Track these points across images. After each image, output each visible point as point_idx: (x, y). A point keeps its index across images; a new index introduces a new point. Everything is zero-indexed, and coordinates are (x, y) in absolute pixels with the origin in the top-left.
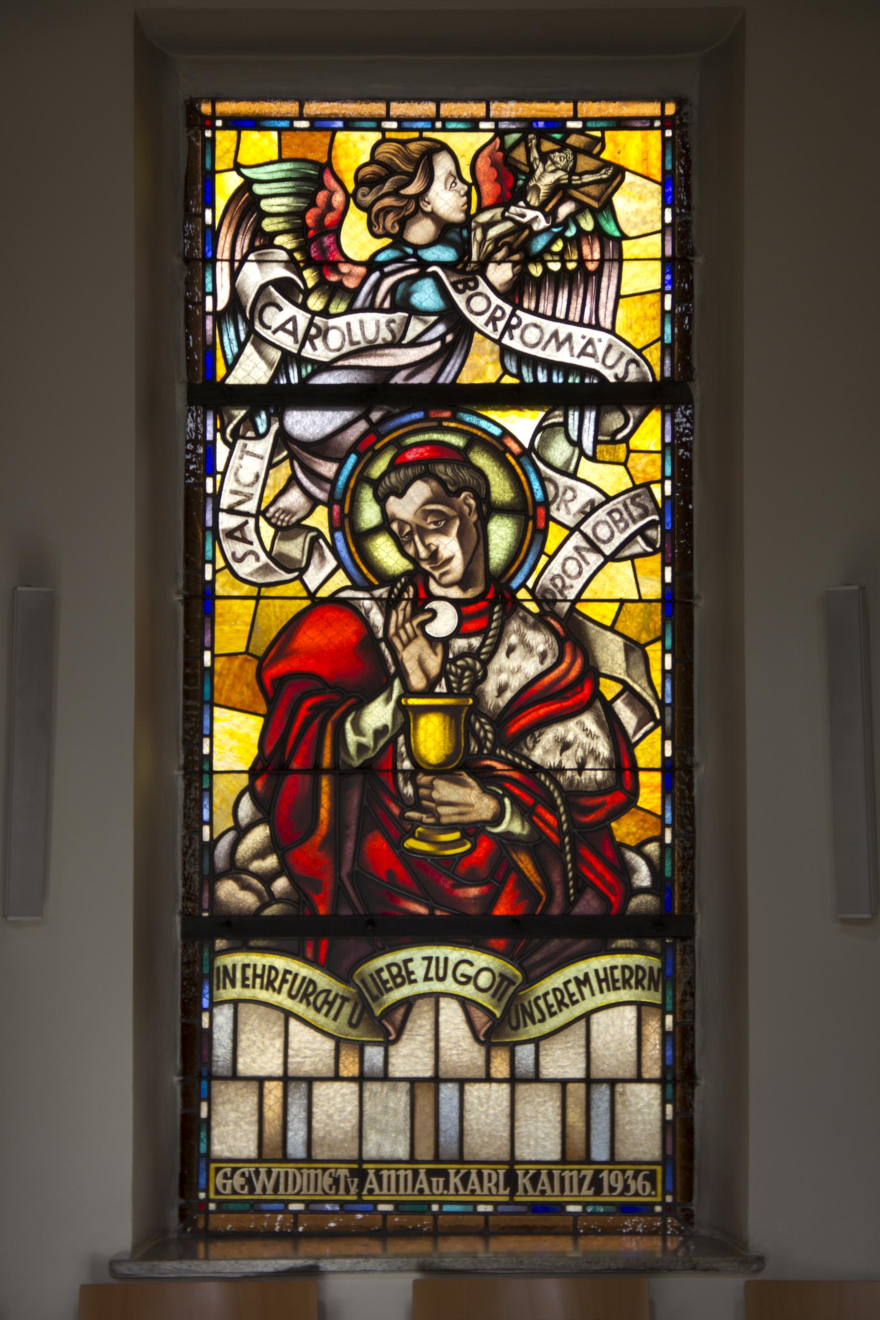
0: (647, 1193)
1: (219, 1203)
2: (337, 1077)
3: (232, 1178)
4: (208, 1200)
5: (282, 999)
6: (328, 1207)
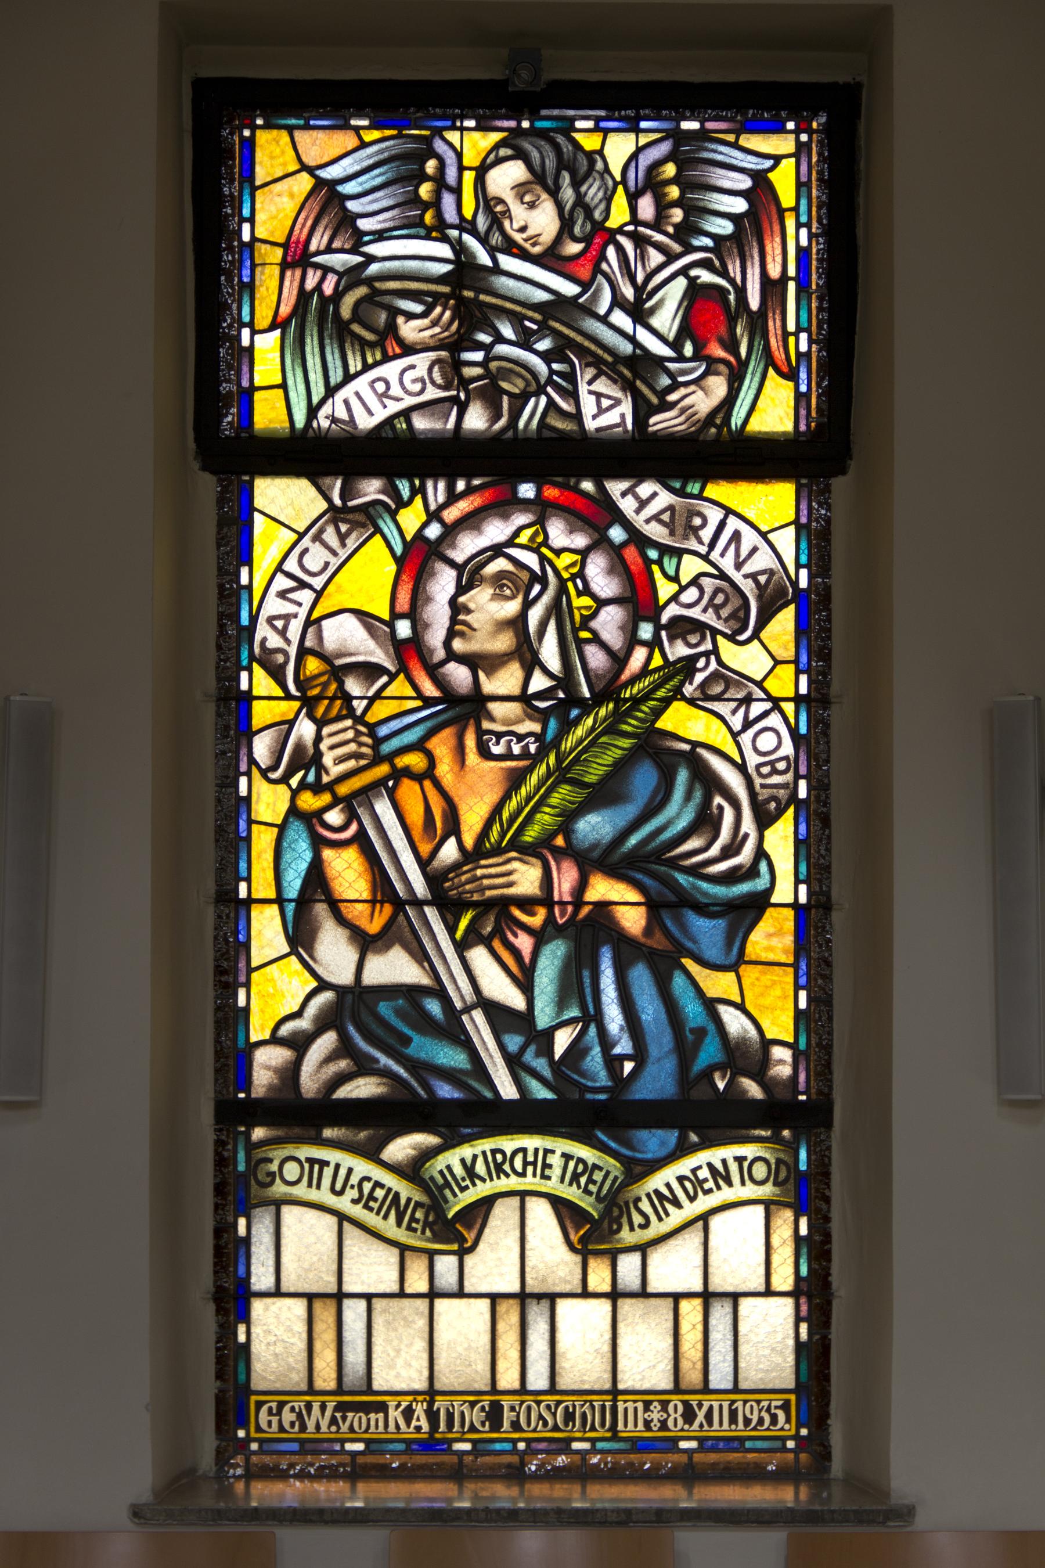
0: (679, 1427)
1: (261, 1442)
2: (585, 1294)
3: (279, 1413)
4: (248, 1439)
5: (344, 1203)
6: (498, 1446)
